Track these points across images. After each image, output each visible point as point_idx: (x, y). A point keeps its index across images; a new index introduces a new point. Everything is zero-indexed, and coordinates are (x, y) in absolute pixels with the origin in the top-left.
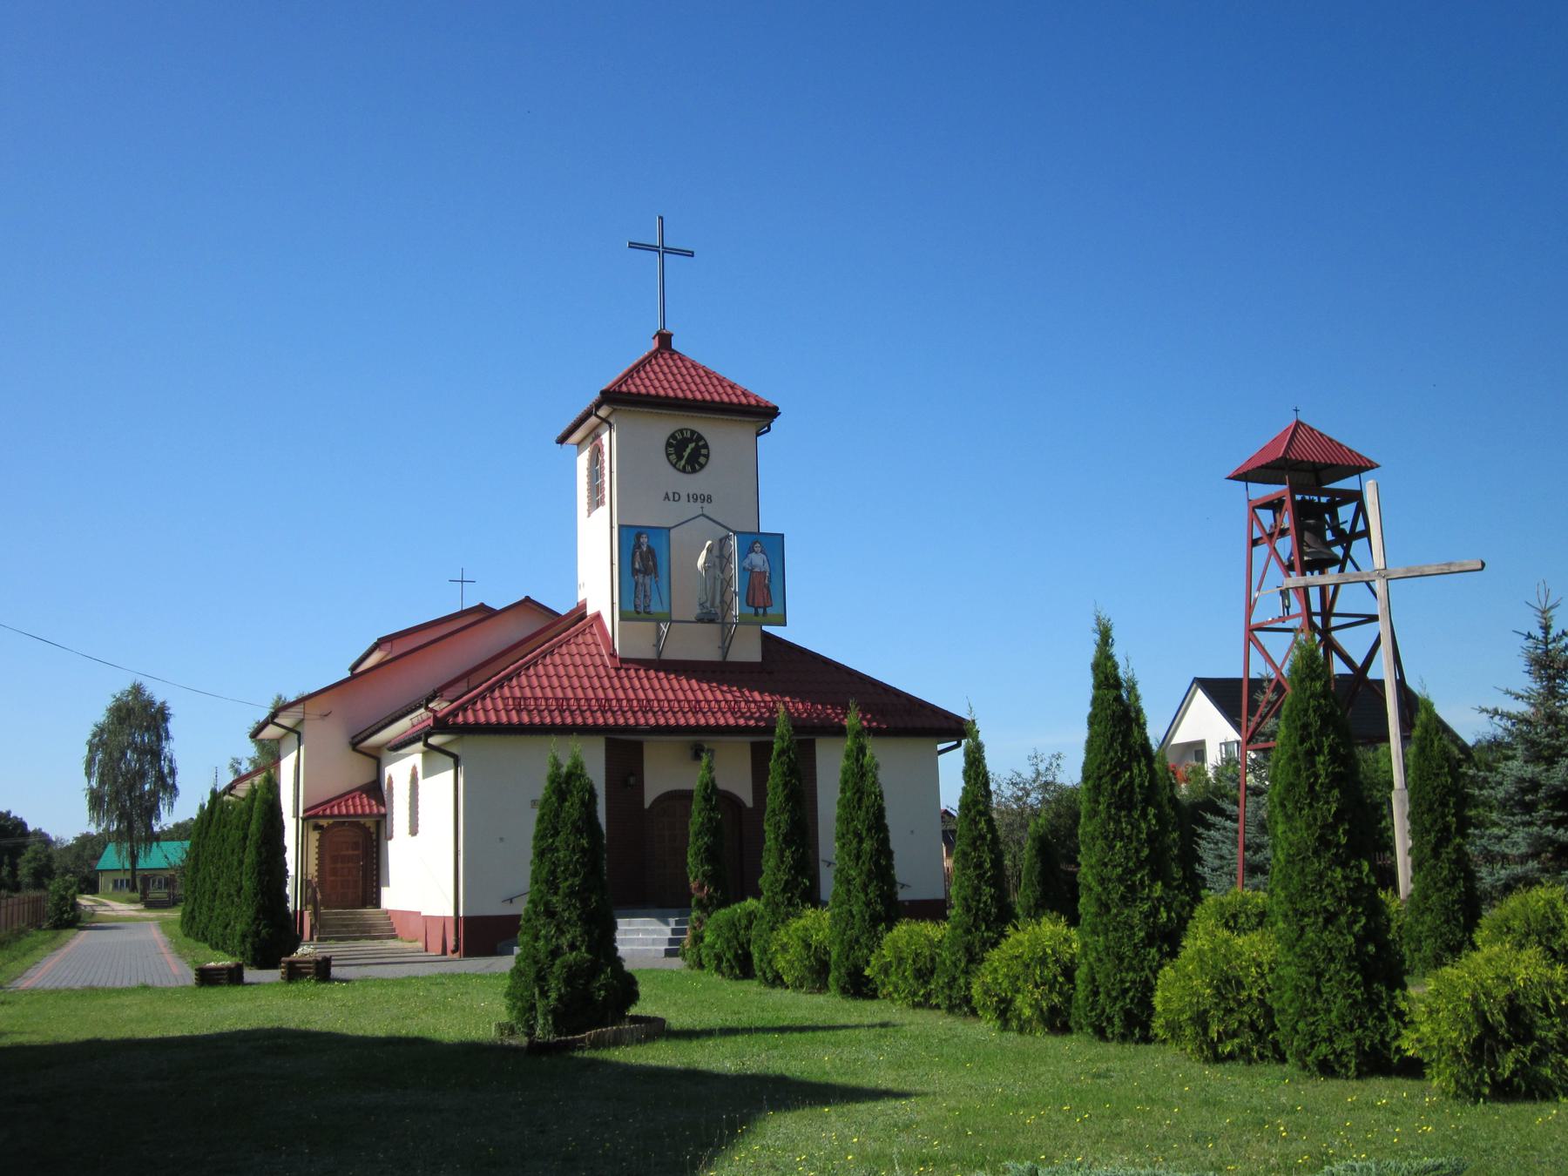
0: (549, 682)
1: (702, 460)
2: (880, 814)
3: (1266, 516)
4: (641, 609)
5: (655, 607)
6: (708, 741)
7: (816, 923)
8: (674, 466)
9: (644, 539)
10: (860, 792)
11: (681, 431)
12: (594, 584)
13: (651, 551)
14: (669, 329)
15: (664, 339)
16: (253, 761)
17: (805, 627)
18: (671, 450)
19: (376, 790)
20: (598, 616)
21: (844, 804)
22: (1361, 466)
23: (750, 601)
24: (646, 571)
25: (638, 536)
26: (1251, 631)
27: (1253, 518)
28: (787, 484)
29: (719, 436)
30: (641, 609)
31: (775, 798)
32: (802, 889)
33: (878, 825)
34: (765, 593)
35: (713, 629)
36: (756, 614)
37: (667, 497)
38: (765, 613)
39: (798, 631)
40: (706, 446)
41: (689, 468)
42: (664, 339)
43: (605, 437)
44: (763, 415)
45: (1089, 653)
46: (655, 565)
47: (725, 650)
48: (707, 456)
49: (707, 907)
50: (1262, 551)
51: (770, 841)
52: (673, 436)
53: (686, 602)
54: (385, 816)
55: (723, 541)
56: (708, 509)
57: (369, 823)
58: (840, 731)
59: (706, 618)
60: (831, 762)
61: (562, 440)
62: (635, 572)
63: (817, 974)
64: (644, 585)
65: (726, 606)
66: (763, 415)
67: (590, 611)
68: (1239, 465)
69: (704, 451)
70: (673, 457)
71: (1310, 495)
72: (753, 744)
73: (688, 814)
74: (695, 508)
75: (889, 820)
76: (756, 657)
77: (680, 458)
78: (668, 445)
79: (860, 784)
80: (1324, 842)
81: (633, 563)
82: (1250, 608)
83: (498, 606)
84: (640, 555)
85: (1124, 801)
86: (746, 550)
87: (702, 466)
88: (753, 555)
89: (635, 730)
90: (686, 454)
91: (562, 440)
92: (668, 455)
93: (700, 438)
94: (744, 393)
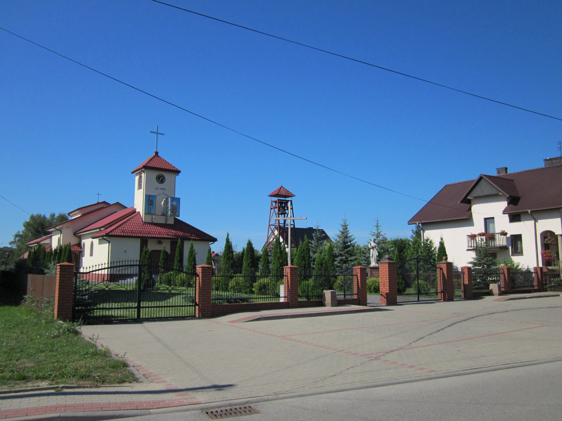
0: (130, 226)
2: (195, 258)
3: (274, 204)
5: (152, 212)
6: (162, 240)
7: (183, 276)
10: (192, 254)
12: (139, 205)
14: (158, 151)
15: (157, 153)
16: (23, 232)
17: (183, 217)
19: (79, 245)
20: (139, 212)
21: (189, 256)
22: (292, 196)
23: (172, 211)
24: (151, 204)
26: (269, 225)
27: (272, 204)
28: (182, 187)
29: (167, 176)
31: (177, 254)
32: (180, 270)
33: (194, 260)
34: (175, 210)
35: (164, 217)
39: (181, 218)
42: (157, 153)
43: (143, 175)
44: (178, 172)
45: (226, 237)
47: (166, 222)
49: (164, 272)
50: (273, 210)
51: (176, 262)
53: (159, 211)
54: (82, 251)
55: (167, 199)
56: (165, 192)
57: (77, 253)
58: (190, 239)
59: (163, 215)
60: (187, 246)
61: (133, 173)
63: (182, 284)
65: (167, 212)
66: (178, 172)
67: (137, 211)
68: (273, 191)
71: (282, 200)
73: (160, 255)
74: (162, 191)
75: (196, 259)
76: (173, 223)
79: (192, 252)
80: (248, 265)
82: (270, 221)
83: (111, 204)
84: (150, 201)
85: (228, 259)
86: (172, 201)
89: (147, 237)
91: (133, 173)
94: (174, 167)
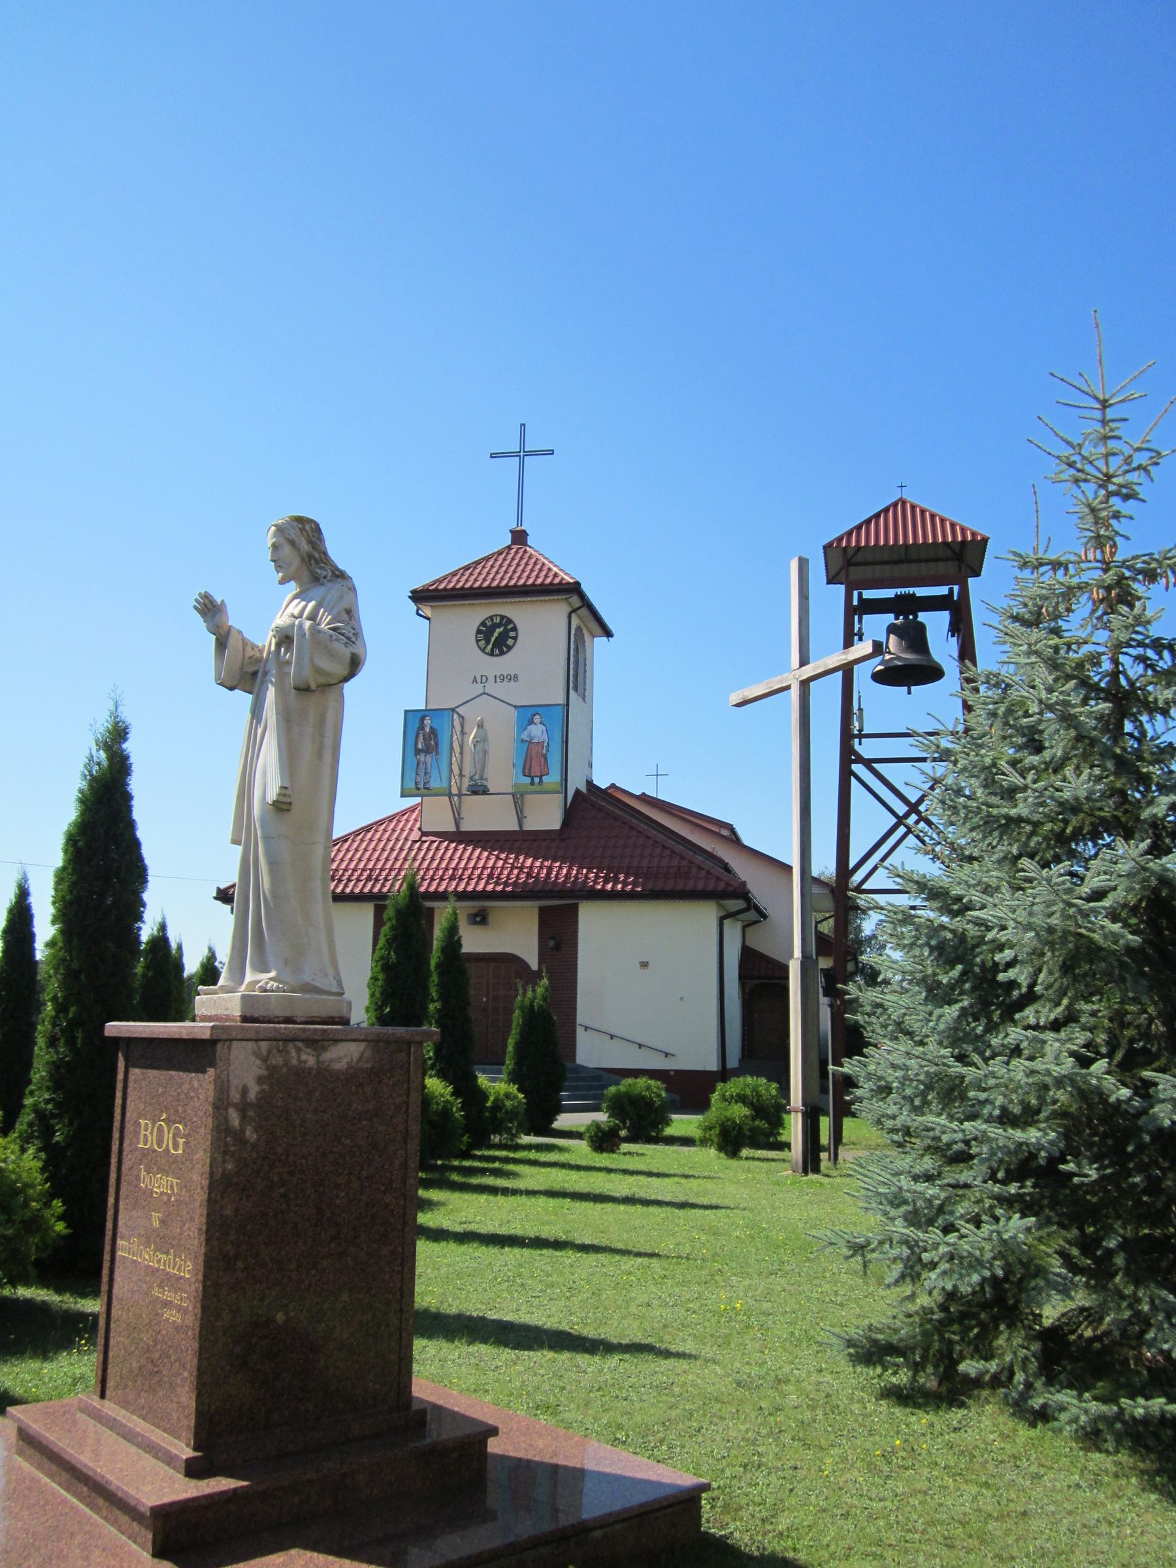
1: (510, 642)
4: (421, 786)
5: (433, 784)
8: (483, 650)
9: (427, 722)
11: (491, 618)
13: (433, 731)
15: (519, 537)
18: (481, 636)
24: (427, 750)
25: (423, 719)
29: (519, 613)
30: (421, 786)
36: (532, 783)
37: (475, 680)
38: (541, 782)
40: (515, 629)
41: (497, 651)
42: (519, 537)
46: (437, 744)
48: (515, 638)
52: (483, 624)
62: (418, 752)
64: (425, 763)
69: (512, 634)
70: (482, 643)
72: (542, 910)
77: (488, 642)
78: (479, 632)
81: (416, 744)
83: (746, 841)
87: (510, 648)
88: (532, 727)
90: (493, 639)
92: (478, 641)
93: (510, 621)
